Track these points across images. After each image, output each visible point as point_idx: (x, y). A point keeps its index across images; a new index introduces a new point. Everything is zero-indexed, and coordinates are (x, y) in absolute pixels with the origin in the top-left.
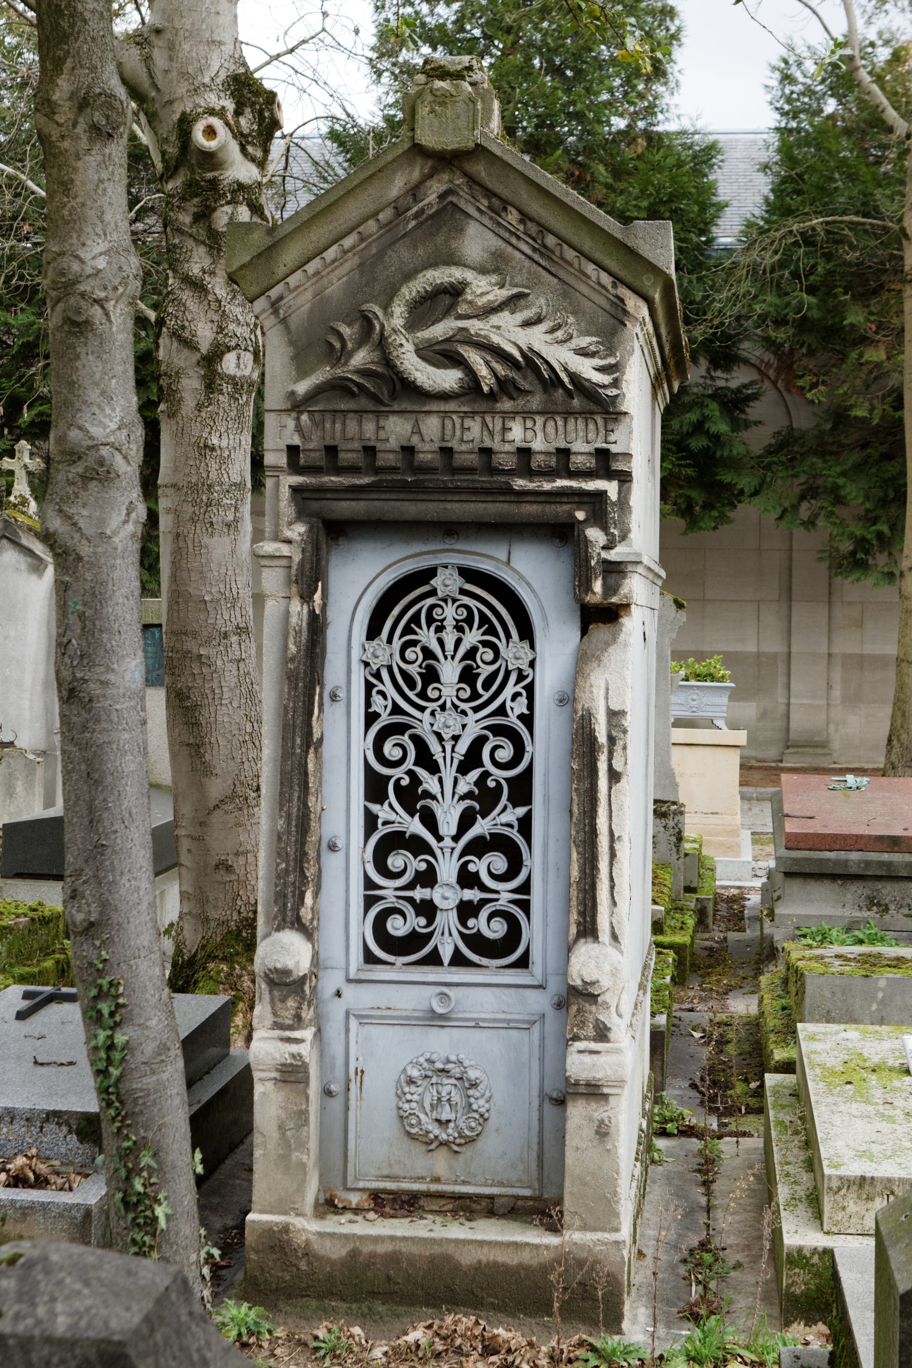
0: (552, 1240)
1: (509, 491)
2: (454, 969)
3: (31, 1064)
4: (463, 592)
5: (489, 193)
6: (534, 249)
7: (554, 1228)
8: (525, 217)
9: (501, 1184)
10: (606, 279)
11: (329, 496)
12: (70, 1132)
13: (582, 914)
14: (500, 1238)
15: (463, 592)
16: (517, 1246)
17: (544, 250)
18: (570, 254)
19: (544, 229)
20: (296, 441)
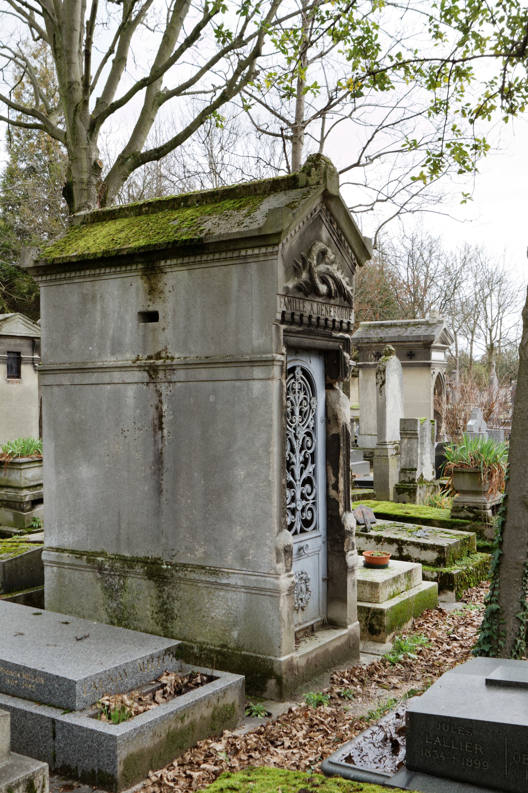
0: (345, 632)
1: (331, 337)
2: (302, 534)
3: (75, 642)
4: (302, 379)
5: (332, 215)
6: (337, 240)
7: (345, 627)
8: (339, 227)
9: (314, 619)
10: (353, 257)
11: (290, 334)
12: (173, 656)
13: (345, 503)
14: (332, 638)
15: (302, 379)
16: (340, 637)
17: (340, 240)
18: (346, 244)
19: (343, 233)
20: (285, 309)
